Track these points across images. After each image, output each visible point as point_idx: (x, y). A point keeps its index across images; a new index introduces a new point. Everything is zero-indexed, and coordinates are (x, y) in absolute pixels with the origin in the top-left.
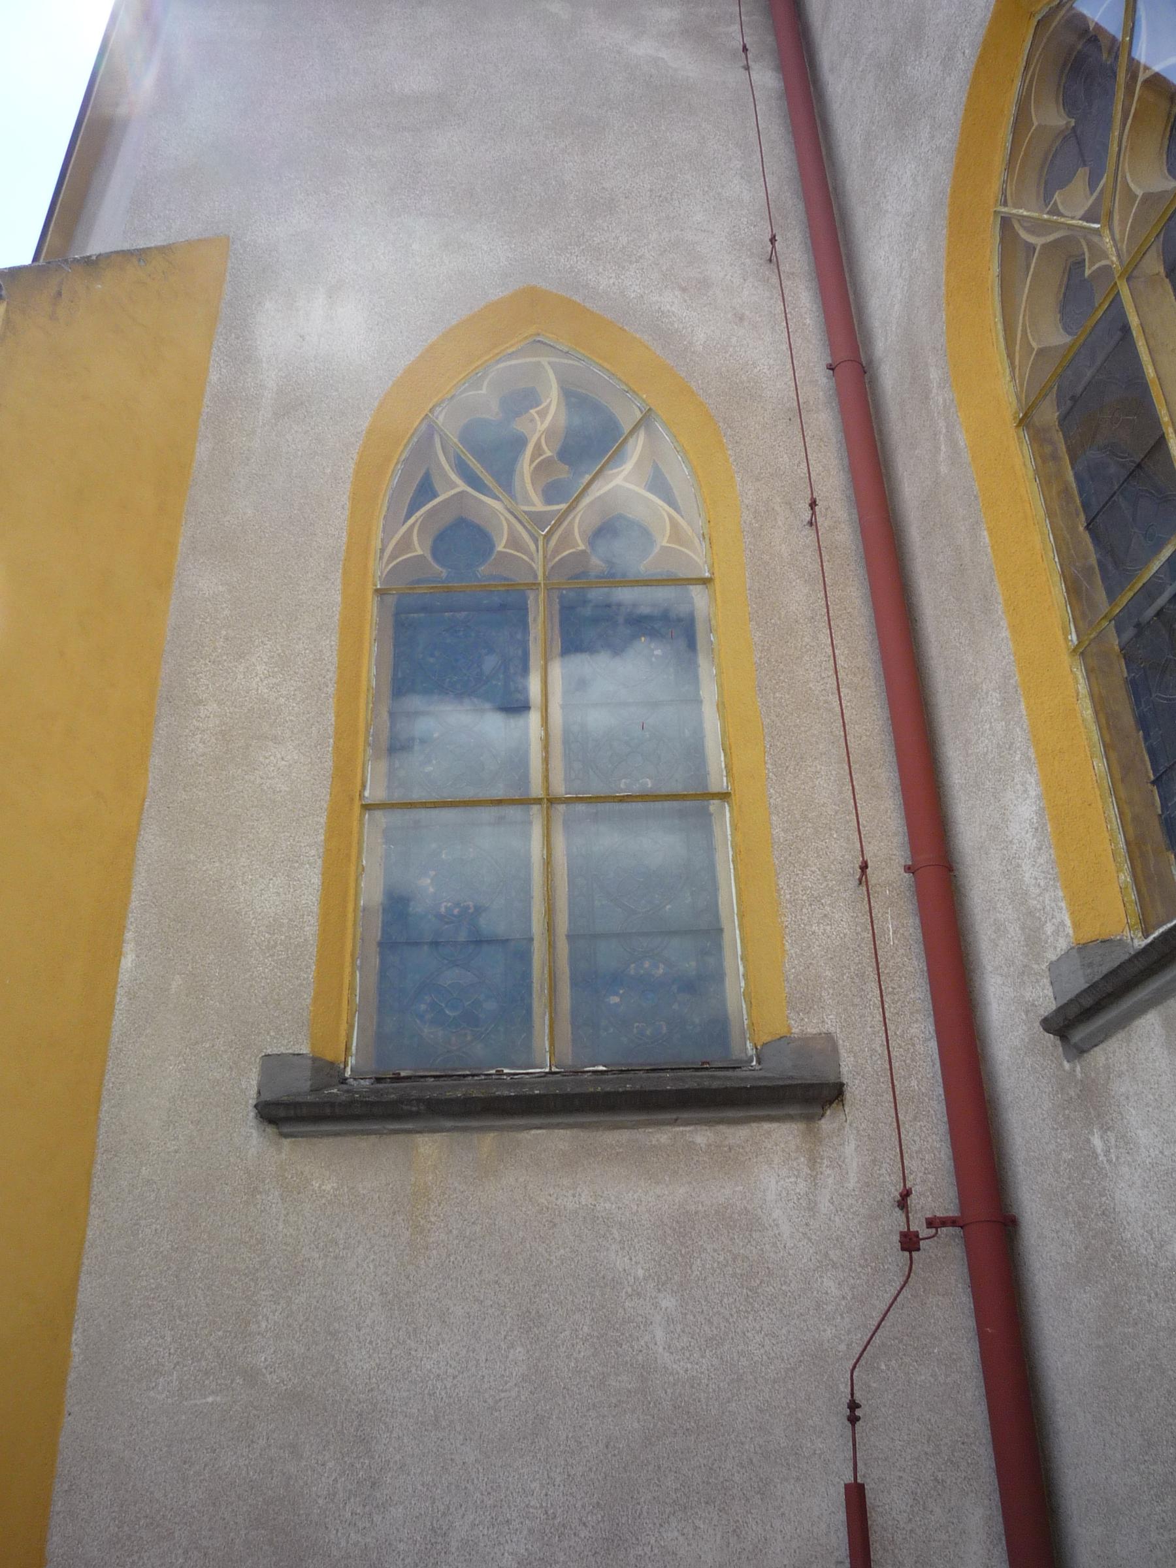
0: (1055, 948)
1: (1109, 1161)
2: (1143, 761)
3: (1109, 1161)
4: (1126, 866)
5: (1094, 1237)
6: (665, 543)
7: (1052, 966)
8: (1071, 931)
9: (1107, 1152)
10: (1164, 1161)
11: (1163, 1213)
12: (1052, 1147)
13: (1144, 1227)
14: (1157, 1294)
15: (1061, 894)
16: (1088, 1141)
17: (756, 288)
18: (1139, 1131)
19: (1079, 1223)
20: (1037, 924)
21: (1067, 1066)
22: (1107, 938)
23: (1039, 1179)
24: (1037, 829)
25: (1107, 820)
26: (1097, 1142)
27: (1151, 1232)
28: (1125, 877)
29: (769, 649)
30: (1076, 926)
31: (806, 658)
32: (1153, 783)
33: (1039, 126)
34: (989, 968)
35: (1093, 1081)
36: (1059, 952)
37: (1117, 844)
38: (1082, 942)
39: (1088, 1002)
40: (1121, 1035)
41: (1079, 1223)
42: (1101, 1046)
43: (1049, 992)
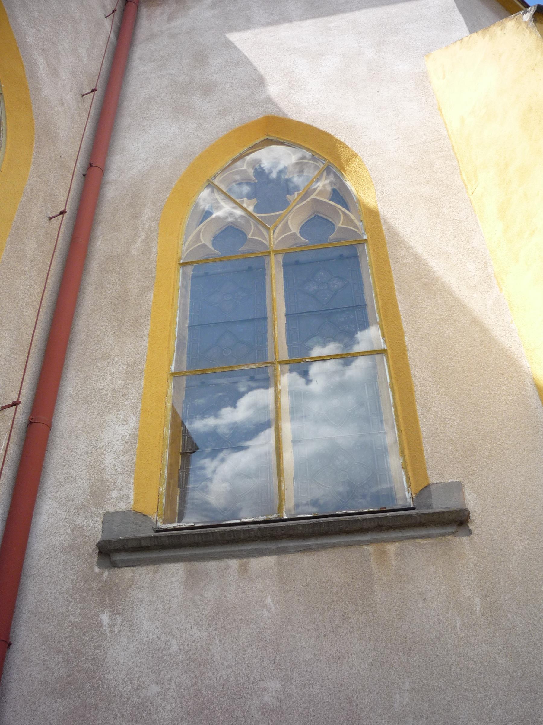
0: (115, 506)
1: (112, 632)
2: (180, 441)
3: (112, 632)
4: (165, 485)
5: (79, 671)
6: (340, 225)
7: (107, 515)
8: (132, 502)
9: (112, 626)
10: (159, 643)
11: (146, 671)
12: (63, 610)
13: (127, 675)
14: (123, 716)
15: (132, 481)
16: (97, 616)
17: (73, 99)
18: (145, 622)
19: (68, 660)
20: (106, 488)
21: (97, 569)
22: (146, 514)
23: (41, 626)
24: (126, 443)
25: (162, 459)
26: (105, 618)
27: (131, 680)
28: (163, 490)
29: (10, 258)
30: (136, 501)
31: (22, 277)
32: (181, 453)
33: (245, 170)
34: (49, 495)
35: (116, 584)
36: (117, 509)
37: (164, 472)
38: (137, 510)
39: (144, 543)
40: (150, 568)
41: (68, 660)
42: (132, 568)
43: (100, 526)
